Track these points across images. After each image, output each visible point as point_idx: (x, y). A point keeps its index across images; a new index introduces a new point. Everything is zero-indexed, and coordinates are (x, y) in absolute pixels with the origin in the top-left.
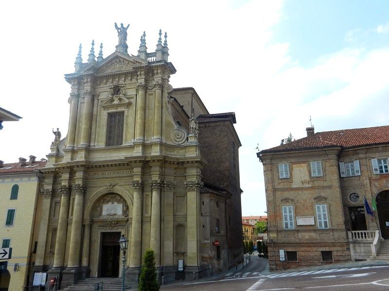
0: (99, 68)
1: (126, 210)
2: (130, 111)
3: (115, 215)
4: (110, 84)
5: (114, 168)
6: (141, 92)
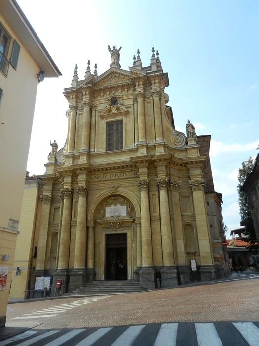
0: (96, 83)
1: (131, 210)
2: (128, 118)
3: (119, 216)
4: (107, 96)
5: (117, 170)
6: (140, 100)
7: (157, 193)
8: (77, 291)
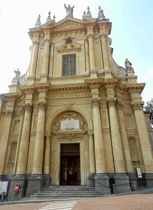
1: (84, 123)
3: (72, 129)
4: (64, 37)
6: (90, 40)
7: (106, 110)
8: (35, 196)
